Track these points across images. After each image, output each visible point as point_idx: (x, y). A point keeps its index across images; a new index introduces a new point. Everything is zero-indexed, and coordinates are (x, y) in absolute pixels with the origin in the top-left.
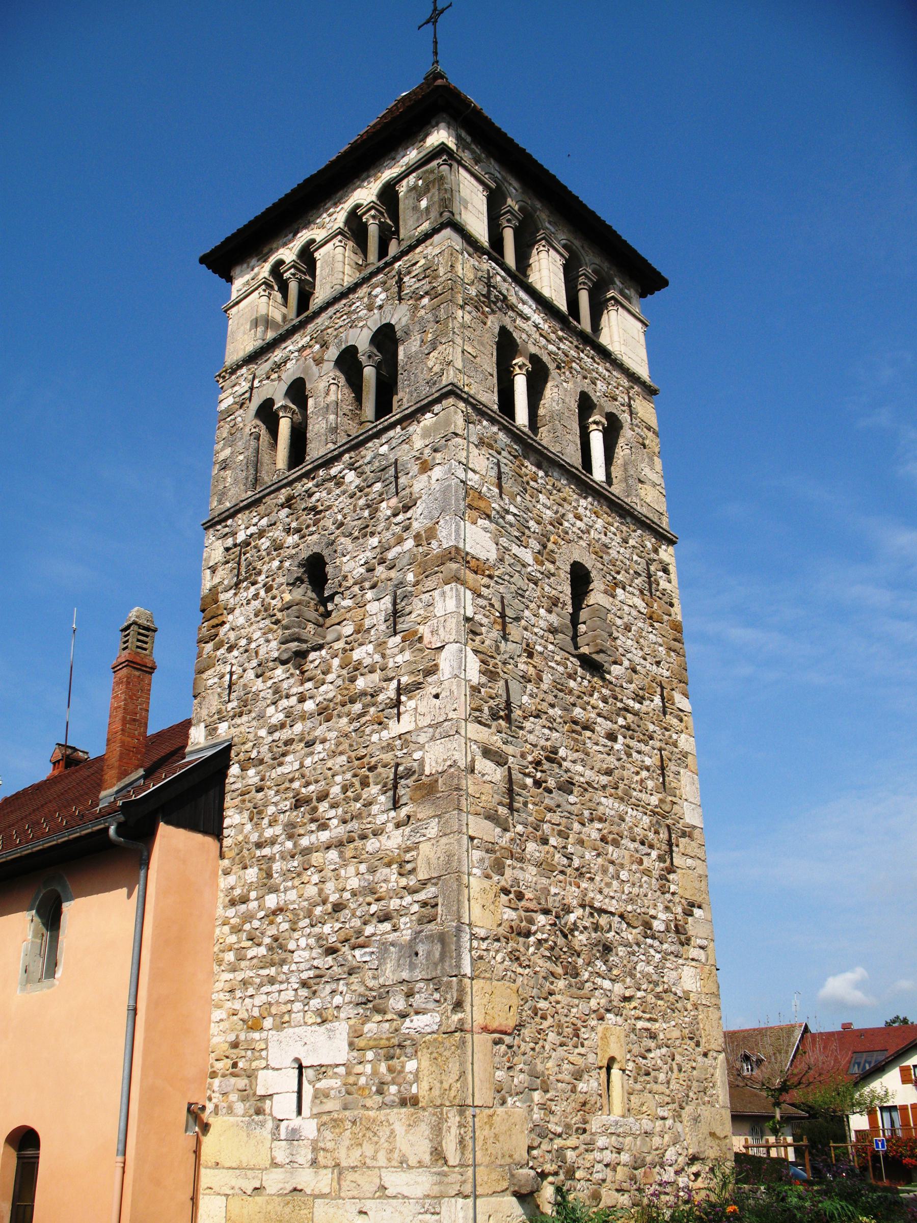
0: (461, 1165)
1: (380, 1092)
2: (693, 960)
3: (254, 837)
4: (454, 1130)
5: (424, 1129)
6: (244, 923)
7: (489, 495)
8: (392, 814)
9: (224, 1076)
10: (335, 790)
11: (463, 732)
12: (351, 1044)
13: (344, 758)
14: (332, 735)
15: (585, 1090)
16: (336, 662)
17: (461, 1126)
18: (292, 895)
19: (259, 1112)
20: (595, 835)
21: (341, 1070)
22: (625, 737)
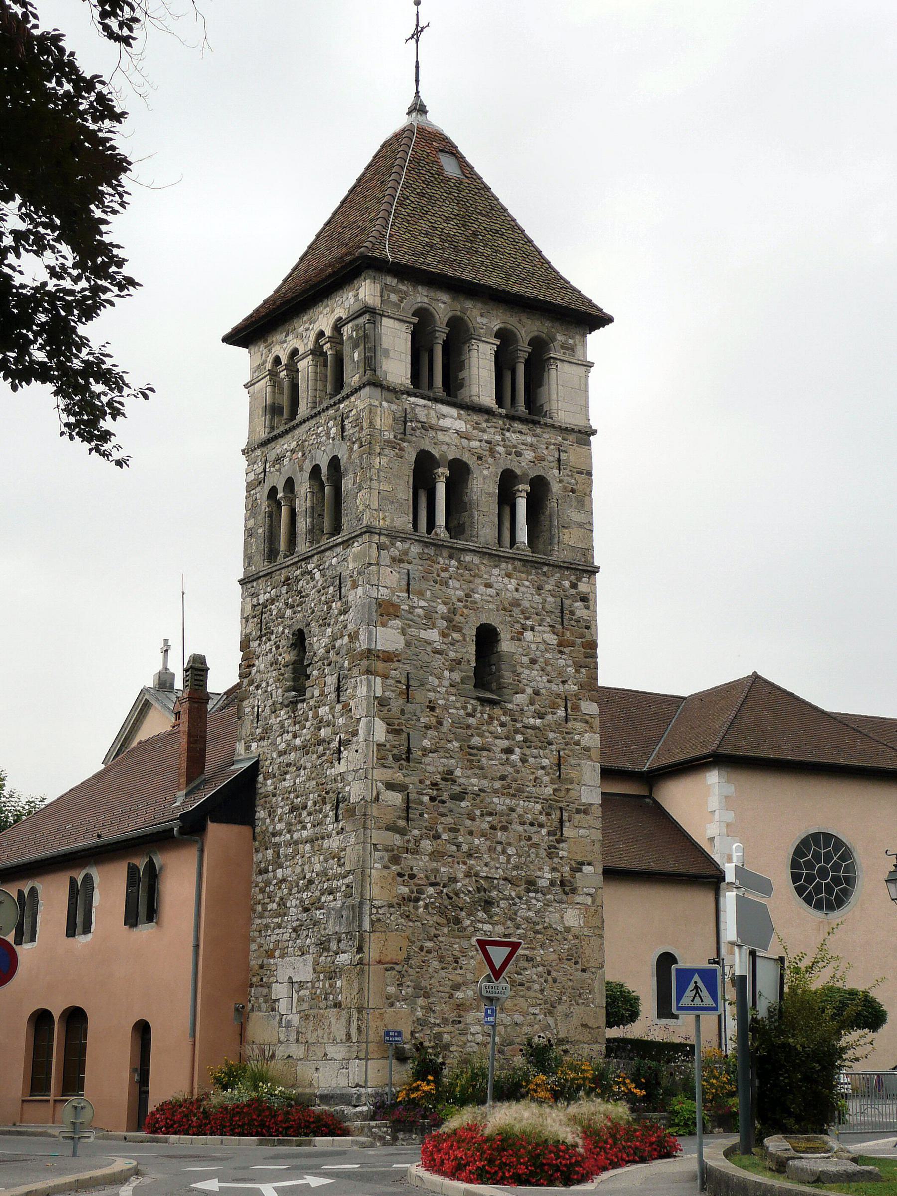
0: (358, 1042)
1: (326, 999)
2: (577, 903)
3: (270, 829)
4: (355, 1022)
5: (343, 1021)
6: (266, 886)
7: (399, 601)
8: (335, 825)
9: (256, 986)
10: (310, 804)
11: (370, 777)
12: (314, 969)
13: (314, 783)
14: (309, 765)
15: (461, 996)
16: (311, 714)
17: (359, 1019)
18: (288, 871)
19: (273, 1009)
20: (486, 826)
21: (309, 985)
22: (521, 748)
